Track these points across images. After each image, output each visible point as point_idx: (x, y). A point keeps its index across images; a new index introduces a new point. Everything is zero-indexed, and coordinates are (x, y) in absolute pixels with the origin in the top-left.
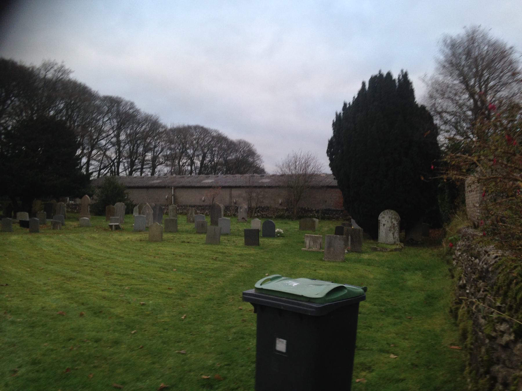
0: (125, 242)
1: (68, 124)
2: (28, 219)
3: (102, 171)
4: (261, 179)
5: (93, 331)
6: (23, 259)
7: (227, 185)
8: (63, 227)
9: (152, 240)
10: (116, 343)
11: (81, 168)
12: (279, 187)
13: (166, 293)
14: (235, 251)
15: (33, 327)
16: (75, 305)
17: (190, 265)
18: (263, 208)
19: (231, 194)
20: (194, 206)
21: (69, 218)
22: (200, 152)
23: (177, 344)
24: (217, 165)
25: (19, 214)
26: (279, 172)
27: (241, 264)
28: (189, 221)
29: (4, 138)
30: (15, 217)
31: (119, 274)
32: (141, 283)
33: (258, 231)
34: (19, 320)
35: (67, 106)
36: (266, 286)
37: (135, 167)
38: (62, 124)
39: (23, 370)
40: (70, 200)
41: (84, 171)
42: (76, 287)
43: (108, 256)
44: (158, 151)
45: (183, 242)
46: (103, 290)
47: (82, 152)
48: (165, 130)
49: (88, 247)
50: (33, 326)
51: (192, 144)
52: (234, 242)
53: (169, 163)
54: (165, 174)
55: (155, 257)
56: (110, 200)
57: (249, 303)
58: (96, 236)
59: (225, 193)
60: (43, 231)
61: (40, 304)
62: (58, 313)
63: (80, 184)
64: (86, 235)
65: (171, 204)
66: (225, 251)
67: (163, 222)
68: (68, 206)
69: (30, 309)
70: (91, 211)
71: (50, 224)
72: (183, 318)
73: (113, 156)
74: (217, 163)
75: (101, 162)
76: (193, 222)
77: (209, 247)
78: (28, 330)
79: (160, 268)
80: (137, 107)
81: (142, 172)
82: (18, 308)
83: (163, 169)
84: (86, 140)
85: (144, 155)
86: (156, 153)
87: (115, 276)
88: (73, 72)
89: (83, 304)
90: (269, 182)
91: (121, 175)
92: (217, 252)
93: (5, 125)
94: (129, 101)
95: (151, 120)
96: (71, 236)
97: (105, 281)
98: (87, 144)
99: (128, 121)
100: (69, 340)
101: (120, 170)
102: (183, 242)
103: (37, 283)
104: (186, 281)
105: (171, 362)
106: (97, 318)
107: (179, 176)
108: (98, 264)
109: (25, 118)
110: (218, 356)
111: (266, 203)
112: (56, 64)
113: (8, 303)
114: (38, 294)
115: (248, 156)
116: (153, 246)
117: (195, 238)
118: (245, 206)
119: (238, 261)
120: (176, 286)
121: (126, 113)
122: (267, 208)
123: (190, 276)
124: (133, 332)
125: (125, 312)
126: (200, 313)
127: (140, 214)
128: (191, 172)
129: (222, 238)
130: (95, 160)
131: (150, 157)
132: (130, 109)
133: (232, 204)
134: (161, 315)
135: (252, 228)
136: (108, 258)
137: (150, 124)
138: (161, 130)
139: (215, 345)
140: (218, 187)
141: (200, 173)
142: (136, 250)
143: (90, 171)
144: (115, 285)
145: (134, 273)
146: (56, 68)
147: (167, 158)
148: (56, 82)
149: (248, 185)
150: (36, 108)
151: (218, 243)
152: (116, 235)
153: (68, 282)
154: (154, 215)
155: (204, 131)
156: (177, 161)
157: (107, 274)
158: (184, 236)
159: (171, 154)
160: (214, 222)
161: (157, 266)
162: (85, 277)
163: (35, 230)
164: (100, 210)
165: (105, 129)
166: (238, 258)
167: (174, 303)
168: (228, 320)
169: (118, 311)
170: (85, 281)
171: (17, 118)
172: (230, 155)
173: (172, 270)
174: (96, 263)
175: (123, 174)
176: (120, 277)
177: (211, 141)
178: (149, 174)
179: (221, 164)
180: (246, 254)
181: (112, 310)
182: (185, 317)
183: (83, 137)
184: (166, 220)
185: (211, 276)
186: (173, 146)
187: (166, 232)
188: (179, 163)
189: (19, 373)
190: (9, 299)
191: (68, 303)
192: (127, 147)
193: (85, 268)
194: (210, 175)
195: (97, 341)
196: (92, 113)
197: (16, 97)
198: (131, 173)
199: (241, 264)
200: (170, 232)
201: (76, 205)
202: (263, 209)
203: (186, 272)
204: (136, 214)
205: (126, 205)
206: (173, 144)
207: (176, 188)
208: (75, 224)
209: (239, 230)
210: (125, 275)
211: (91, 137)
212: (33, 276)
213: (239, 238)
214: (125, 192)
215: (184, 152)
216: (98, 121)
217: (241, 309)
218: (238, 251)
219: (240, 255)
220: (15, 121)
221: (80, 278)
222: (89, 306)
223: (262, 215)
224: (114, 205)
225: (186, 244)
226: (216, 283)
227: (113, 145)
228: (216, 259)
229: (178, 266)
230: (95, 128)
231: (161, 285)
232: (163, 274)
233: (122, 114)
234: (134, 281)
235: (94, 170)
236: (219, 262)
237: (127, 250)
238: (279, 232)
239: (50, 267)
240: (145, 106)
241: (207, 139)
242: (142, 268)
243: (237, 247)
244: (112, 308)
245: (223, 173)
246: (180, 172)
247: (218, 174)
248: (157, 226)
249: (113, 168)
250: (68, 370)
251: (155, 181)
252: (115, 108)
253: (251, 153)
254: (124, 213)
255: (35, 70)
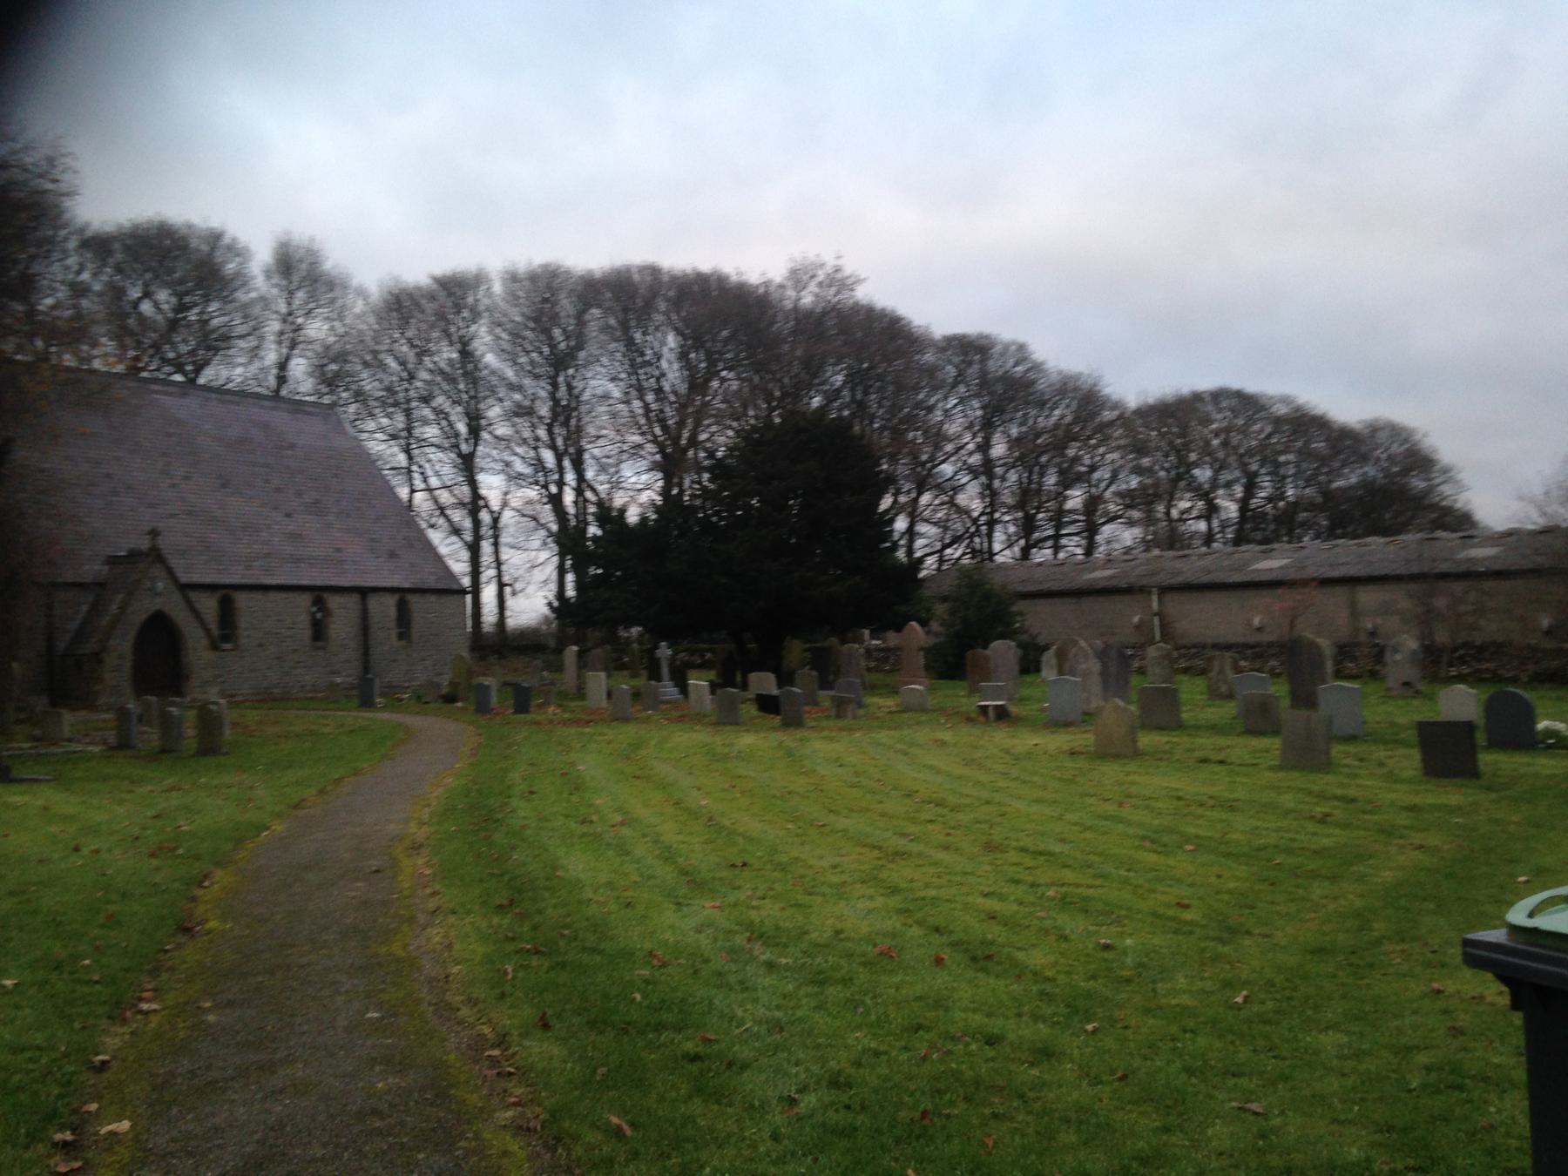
0: (1029, 755)
1: (857, 428)
2: (775, 692)
3: (948, 551)
4: (1465, 547)
5: (975, 1011)
6: (774, 797)
7: (1336, 573)
8: (861, 712)
9: (1105, 752)
10: (1045, 1054)
11: (895, 546)
12: (1536, 572)
13: (1173, 919)
14: (1393, 796)
15: (821, 983)
16: (915, 931)
17: (1235, 836)
18: (1481, 649)
19: (1353, 604)
20: (1228, 647)
21: (872, 688)
22: (1237, 473)
23: (1231, 1082)
24: (1295, 513)
25: (754, 677)
26: (1533, 520)
27: (1418, 838)
28: (1216, 695)
29: (710, 480)
30: (744, 686)
31: (1023, 850)
32: (1090, 882)
33: (1469, 727)
34: (784, 961)
35: (853, 379)
36: (1546, 922)
37: (1036, 535)
38: (842, 426)
39: (809, 1101)
40: (873, 638)
41: (901, 554)
42: (912, 881)
43: (985, 794)
44: (1100, 480)
45: (1205, 761)
46: (986, 895)
47: (895, 502)
48: (1119, 417)
49: (931, 768)
50: (820, 980)
51: (1207, 450)
52: (1381, 764)
53: (1136, 514)
54: (1128, 550)
55: (1121, 804)
56: (976, 632)
57: (1489, 976)
58: (947, 736)
59: (1333, 604)
60: (813, 724)
61: (829, 922)
62: (877, 950)
63: (890, 591)
64: (923, 735)
65: (1152, 642)
66: (1352, 792)
67: (1134, 696)
68: (868, 651)
69: (807, 933)
70: (927, 667)
71: (827, 704)
72: (1239, 1000)
73: (976, 506)
74: (1295, 504)
75: (943, 525)
76: (1230, 696)
77: (1296, 778)
78: (810, 989)
79: (1144, 838)
80: (1034, 357)
81: (1057, 548)
82: (777, 928)
83: (1120, 536)
84: (902, 469)
85: (1061, 497)
86: (1097, 486)
87: (1013, 856)
88: (864, 280)
89: (937, 930)
90: (1495, 557)
91: (999, 559)
92: (1322, 796)
93: (708, 445)
94: (1013, 343)
95: (1076, 389)
96: (883, 736)
97: (988, 868)
98: (906, 477)
99: (1012, 399)
100: (919, 1028)
101: (997, 547)
102: (1205, 761)
103: (814, 862)
104: (1232, 885)
105: (1220, 1133)
106: (981, 975)
107: (1171, 553)
108: (964, 818)
109: (753, 422)
110: (1378, 1137)
111: (1490, 629)
112: (822, 265)
113: (753, 914)
114: (824, 895)
115: (1406, 472)
116: (1111, 772)
117: (1242, 747)
118: (1412, 644)
119: (1406, 827)
120: (1200, 898)
121: (1008, 380)
122: (1495, 649)
123: (1242, 871)
124: (1090, 1027)
125: (1056, 963)
126: (1295, 989)
127: (1061, 673)
128: (1209, 538)
129: (1337, 750)
130: (927, 521)
131: (1078, 500)
132: (1017, 364)
133: (1363, 638)
134: (1169, 986)
135: (1439, 719)
136: (988, 803)
137: (1075, 403)
138: (1108, 415)
139: (1362, 1100)
140: (1305, 583)
141: (1239, 540)
142: (1061, 780)
143: (918, 554)
144: (1017, 882)
145: (1066, 848)
146: (821, 276)
147: (1130, 499)
148: (824, 313)
149: (1415, 569)
150: (777, 394)
151: (1325, 765)
152: (1000, 736)
153: (891, 866)
154: (1104, 673)
155: (1246, 404)
156: (1161, 508)
157: (990, 847)
158: (1206, 743)
159: (1143, 487)
160: (1304, 698)
161: (1131, 831)
162: (932, 852)
163: (793, 722)
164: (953, 662)
165: (951, 431)
166: (1403, 819)
167: (1203, 950)
168: (1396, 1023)
169: (1038, 958)
170: (936, 864)
171: (735, 424)
172: (1339, 476)
173: (1180, 847)
174: (960, 816)
175: (1005, 556)
176: (1028, 861)
177: (1269, 436)
178: (1079, 551)
179: (1311, 506)
180: (1438, 808)
181: (1020, 955)
182: (1246, 998)
183: (893, 459)
184: (1143, 691)
185: (1314, 875)
186: (1146, 462)
187: (1144, 727)
188: (1168, 513)
189: (802, 1108)
190: (754, 903)
191: (898, 925)
192: (1013, 476)
193: (930, 827)
194: (1276, 546)
195: (992, 1041)
196: (917, 388)
197: (730, 369)
198: (1025, 553)
199: (1418, 838)
200: (1160, 728)
201: (888, 650)
202: (1480, 651)
203: (1228, 855)
204: (1049, 673)
205: (1020, 646)
206: (1146, 455)
207: (1165, 590)
208: (890, 702)
209: (1393, 724)
210: (1041, 853)
211: (915, 456)
212: (802, 844)
213: (1402, 751)
214: (1014, 609)
215: (1181, 477)
216: (930, 409)
217: (1439, 992)
218: (1401, 795)
219: (1412, 808)
220: (730, 433)
221: (920, 854)
222: (955, 938)
223: (1479, 671)
224: (985, 648)
225: (1218, 768)
226: (1335, 898)
227: (974, 472)
228: (1323, 820)
229: (1197, 837)
230: (926, 432)
231: (1154, 891)
232: (1153, 858)
233: (995, 379)
234: (1069, 876)
235: (928, 550)
236: (1337, 831)
237: (1035, 778)
238: (1550, 733)
239: (842, 823)
240: (1058, 348)
241: (1256, 427)
242: (1088, 835)
243: (1396, 782)
244: (1020, 949)
245: (1317, 537)
246: (1173, 539)
247: (1300, 539)
248: (1119, 711)
249: (977, 540)
250: (924, 1114)
251: (1098, 574)
252: (976, 367)
253: (1418, 461)
254: (1016, 668)
255: (772, 289)
